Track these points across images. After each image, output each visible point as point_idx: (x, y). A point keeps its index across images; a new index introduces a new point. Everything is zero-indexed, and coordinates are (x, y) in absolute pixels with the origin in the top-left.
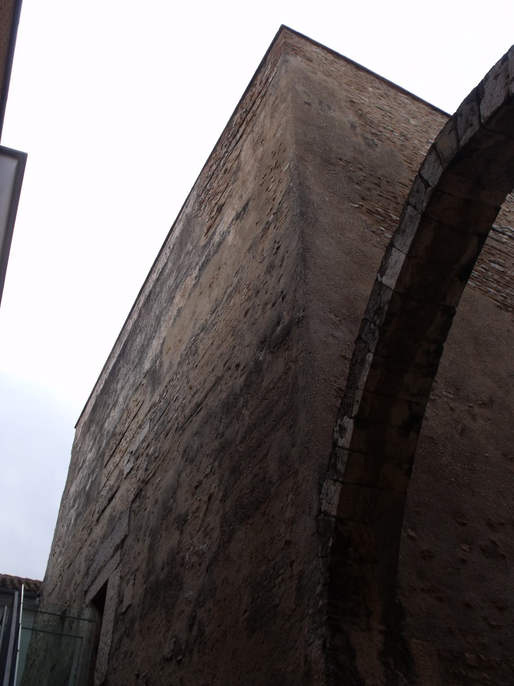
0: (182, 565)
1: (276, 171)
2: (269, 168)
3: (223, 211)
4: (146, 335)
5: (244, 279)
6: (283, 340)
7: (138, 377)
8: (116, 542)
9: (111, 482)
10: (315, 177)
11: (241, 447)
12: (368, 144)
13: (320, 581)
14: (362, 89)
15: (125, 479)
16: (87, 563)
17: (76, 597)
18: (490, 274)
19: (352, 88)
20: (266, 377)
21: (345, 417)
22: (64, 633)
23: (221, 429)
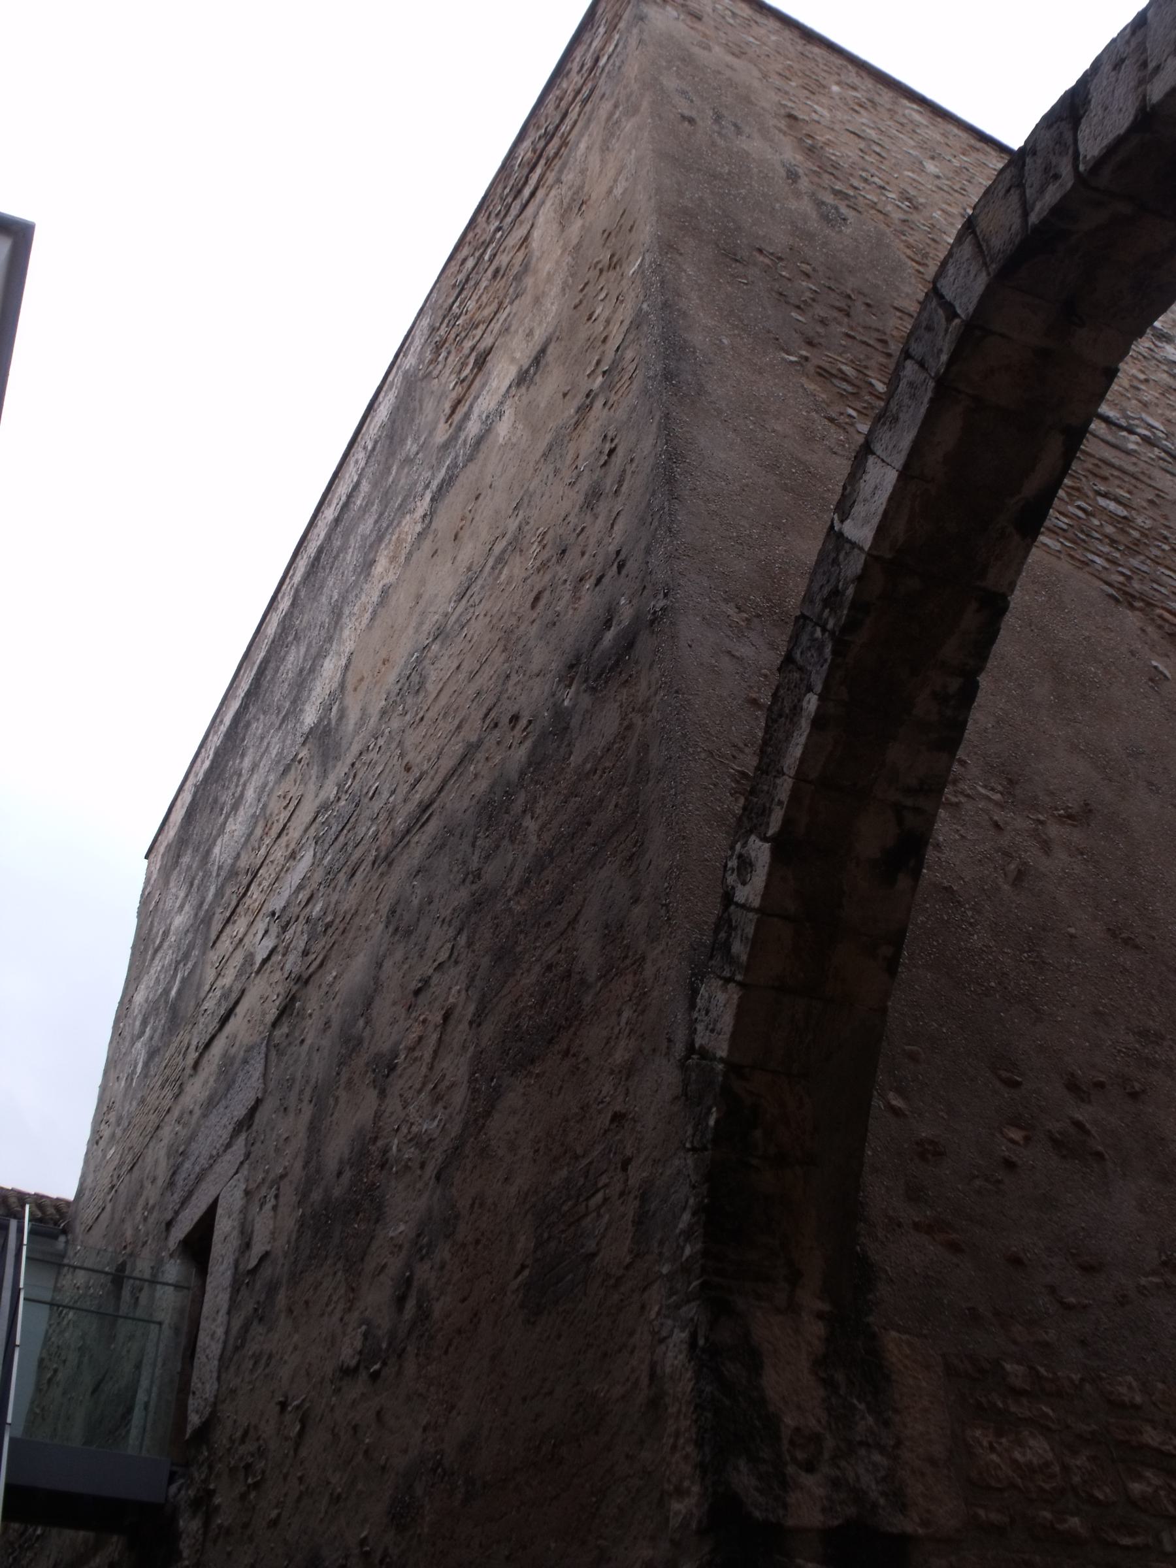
0: (382, 1166)
1: (612, 275)
2: (597, 267)
3: (489, 365)
4: (309, 645)
5: (532, 522)
7: (288, 742)
8: (236, 1113)
9: (227, 980)
10: (700, 290)
11: (518, 902)
12: (825, 218)
13: (687, 1202)
14: (815, 88)
15: (258, 972)
16: (172, 1160)
17: (147, 1235)
18: (1096, 522)
19: (793, 84)
20: (577, 745)
21: (753, 838)
22: (121, 1313)
23: (474, 863)
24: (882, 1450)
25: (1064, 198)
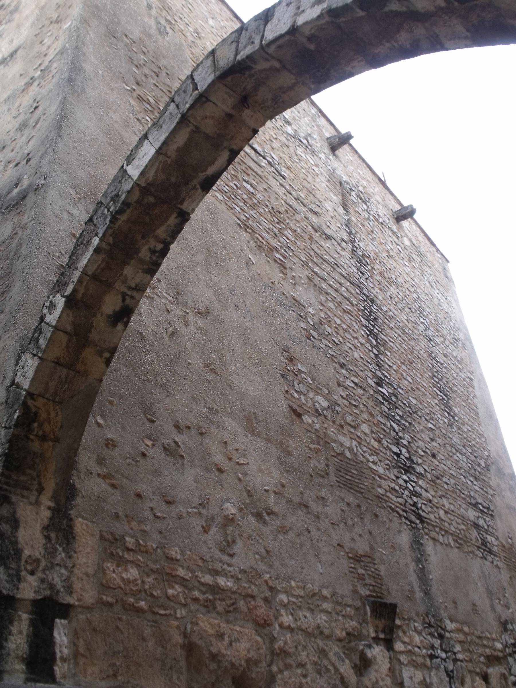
1: (56, 26)
6: (16, 204)
10: (94, 45)
12: (159, 30)
21: (58, 294)
24: (66, 568)
25: (254, 52)
